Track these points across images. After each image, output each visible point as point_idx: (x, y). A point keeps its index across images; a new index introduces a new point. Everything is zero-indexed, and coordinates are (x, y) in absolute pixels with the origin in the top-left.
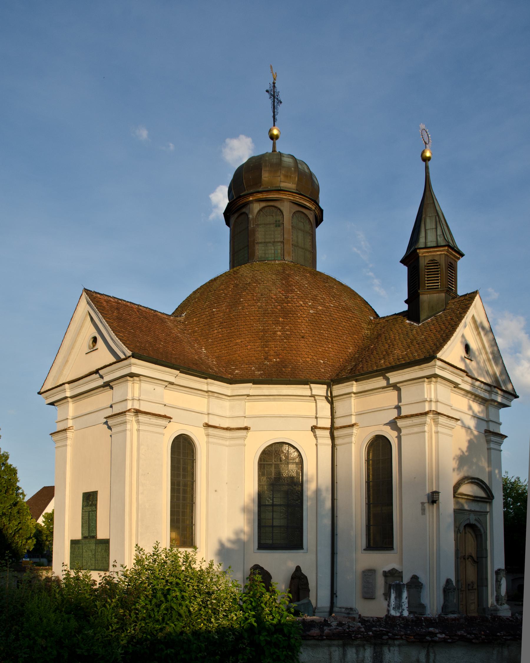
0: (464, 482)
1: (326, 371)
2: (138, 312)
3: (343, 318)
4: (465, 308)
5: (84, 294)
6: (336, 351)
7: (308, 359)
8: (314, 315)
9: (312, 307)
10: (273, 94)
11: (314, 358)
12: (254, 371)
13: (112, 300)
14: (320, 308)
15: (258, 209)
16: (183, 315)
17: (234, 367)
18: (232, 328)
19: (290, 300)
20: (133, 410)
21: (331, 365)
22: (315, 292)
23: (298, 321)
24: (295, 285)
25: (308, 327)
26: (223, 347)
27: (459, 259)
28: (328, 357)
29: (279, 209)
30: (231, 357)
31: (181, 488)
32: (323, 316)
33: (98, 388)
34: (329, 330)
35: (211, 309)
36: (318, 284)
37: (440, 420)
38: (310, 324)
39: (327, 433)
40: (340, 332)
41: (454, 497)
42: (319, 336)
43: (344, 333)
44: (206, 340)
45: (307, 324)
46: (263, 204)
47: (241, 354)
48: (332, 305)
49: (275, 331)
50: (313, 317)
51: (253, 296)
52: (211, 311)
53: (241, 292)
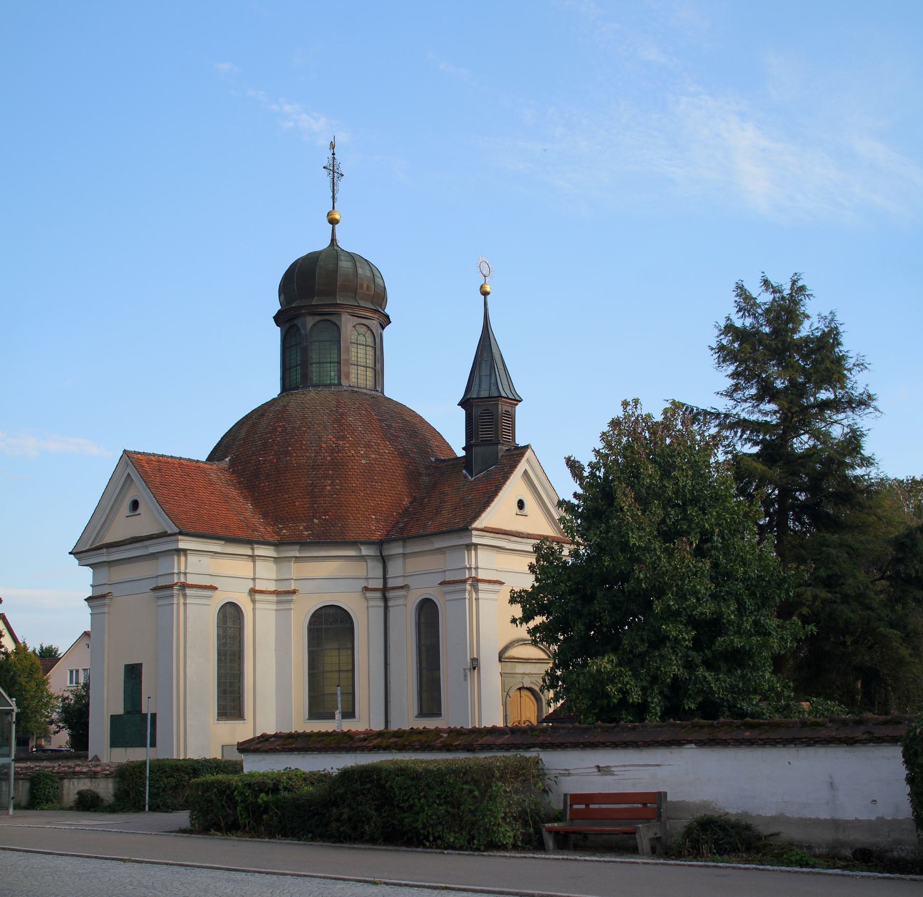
4: (522, 455)
8: (366, 465)
9: (366, 456)
10: (334, 171)
11: (366, 513)
14: (374, 456)
16: (227, 459)
19: (341, 448)
26: (270, 502)
27: (517, 404)
29: (336, 324)
33: (163, 588)
34: (382, 481)
35: (258, 456)
38: (361, 476)
40: (394, 483)
41: (500, 661)
46: (318, 318)
47: (289, 511)
48: (387, 451)
49: (324, 486)
50: (365, 468)
51: (302, 444)
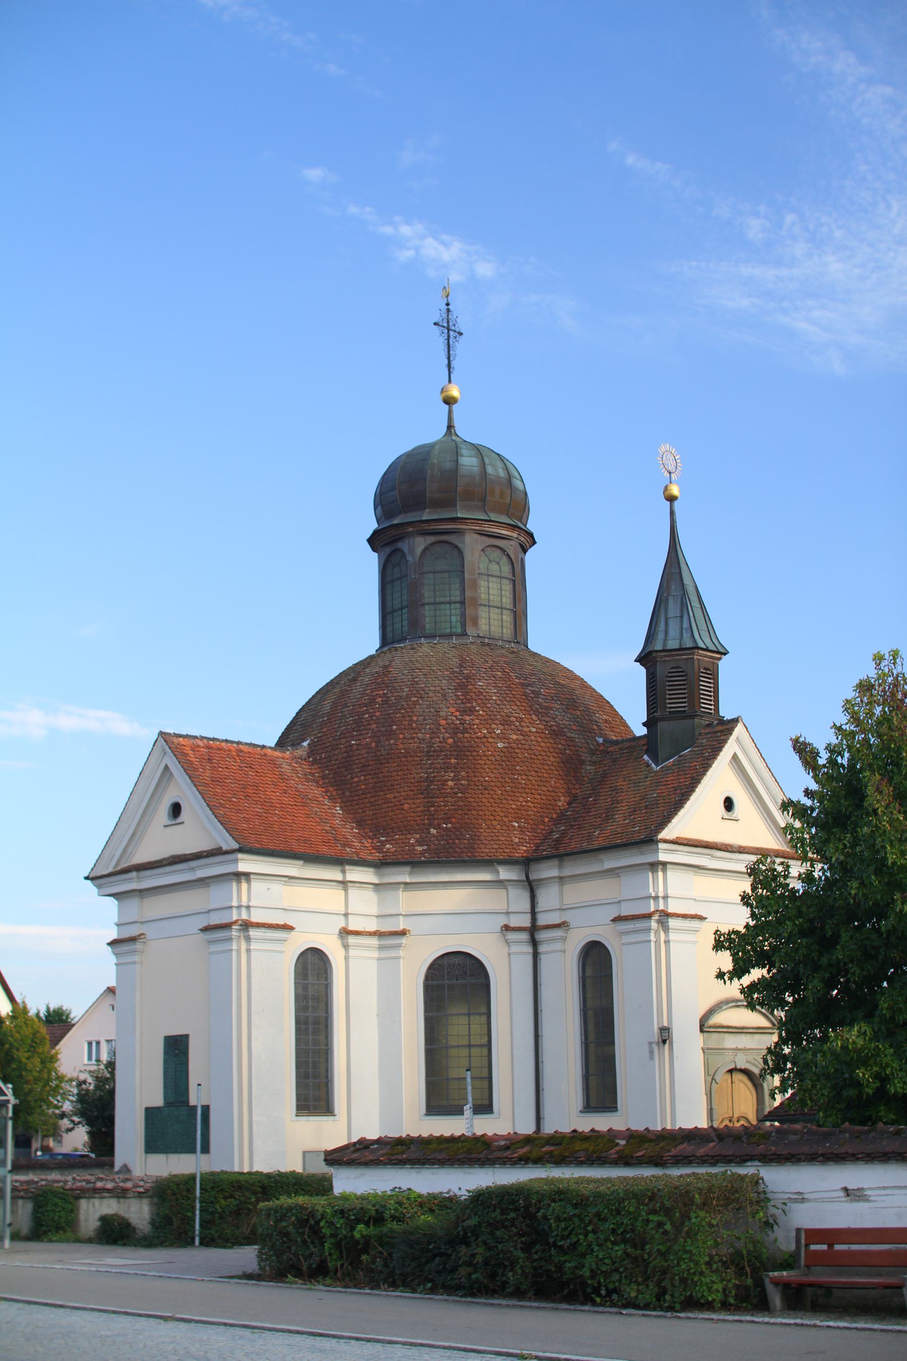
0: (721, 1007)
1: (521, 840)
2: (238, 756)
3: (551, 750)
5: (161, 740)
6: (539, 806)
7: (495, 823)
9: (503, 737)
11: (505, 819)
12: (413, 845)
13: (200, 743)
15: (423, 547)
16: (305, 744)
17: (384, 839)
18: (380, 776)
20: (240, 922)
21: (530, 830)
22: (507, 710)
23: (480, 762)
24: (477, 697)
25: (495, 771)
28: (526, 817)
29: (456, 547)
30: (380, 820)
31: (310, 1027)
32: (519, 751)
34: (528, 773)
36: (513, 692)
37: (670, 923)
38: (497, 767)
39: (525, 936)
40: (545, 775)
41: (702, 1031)
42: (511, 784)
43: (551, 776)
44: (341, 792)
45: (493, 767)
46: (431, 539)
47: (395, 817)
48: (534, 730)
50: (502, 754)
52: (348, 744)
53: (394, 713)
